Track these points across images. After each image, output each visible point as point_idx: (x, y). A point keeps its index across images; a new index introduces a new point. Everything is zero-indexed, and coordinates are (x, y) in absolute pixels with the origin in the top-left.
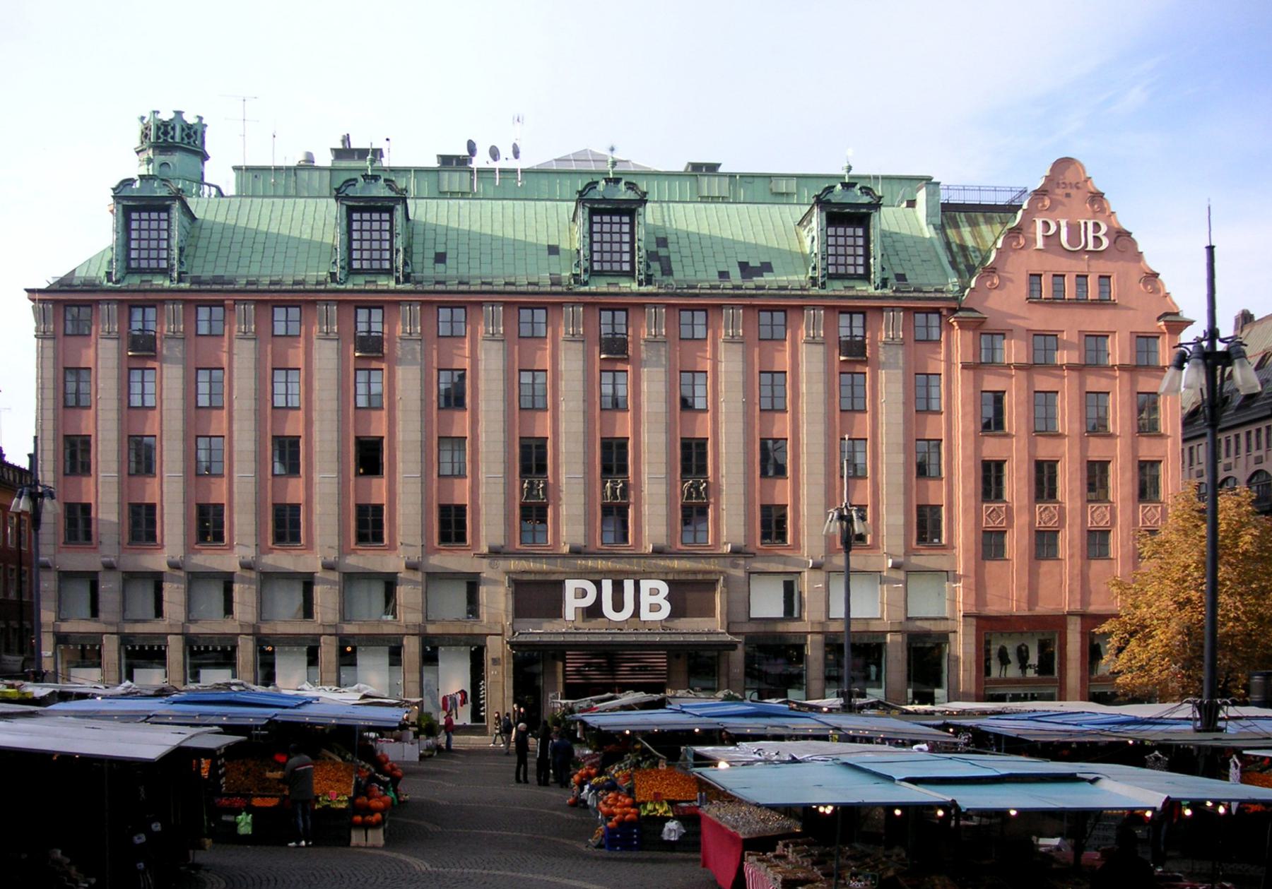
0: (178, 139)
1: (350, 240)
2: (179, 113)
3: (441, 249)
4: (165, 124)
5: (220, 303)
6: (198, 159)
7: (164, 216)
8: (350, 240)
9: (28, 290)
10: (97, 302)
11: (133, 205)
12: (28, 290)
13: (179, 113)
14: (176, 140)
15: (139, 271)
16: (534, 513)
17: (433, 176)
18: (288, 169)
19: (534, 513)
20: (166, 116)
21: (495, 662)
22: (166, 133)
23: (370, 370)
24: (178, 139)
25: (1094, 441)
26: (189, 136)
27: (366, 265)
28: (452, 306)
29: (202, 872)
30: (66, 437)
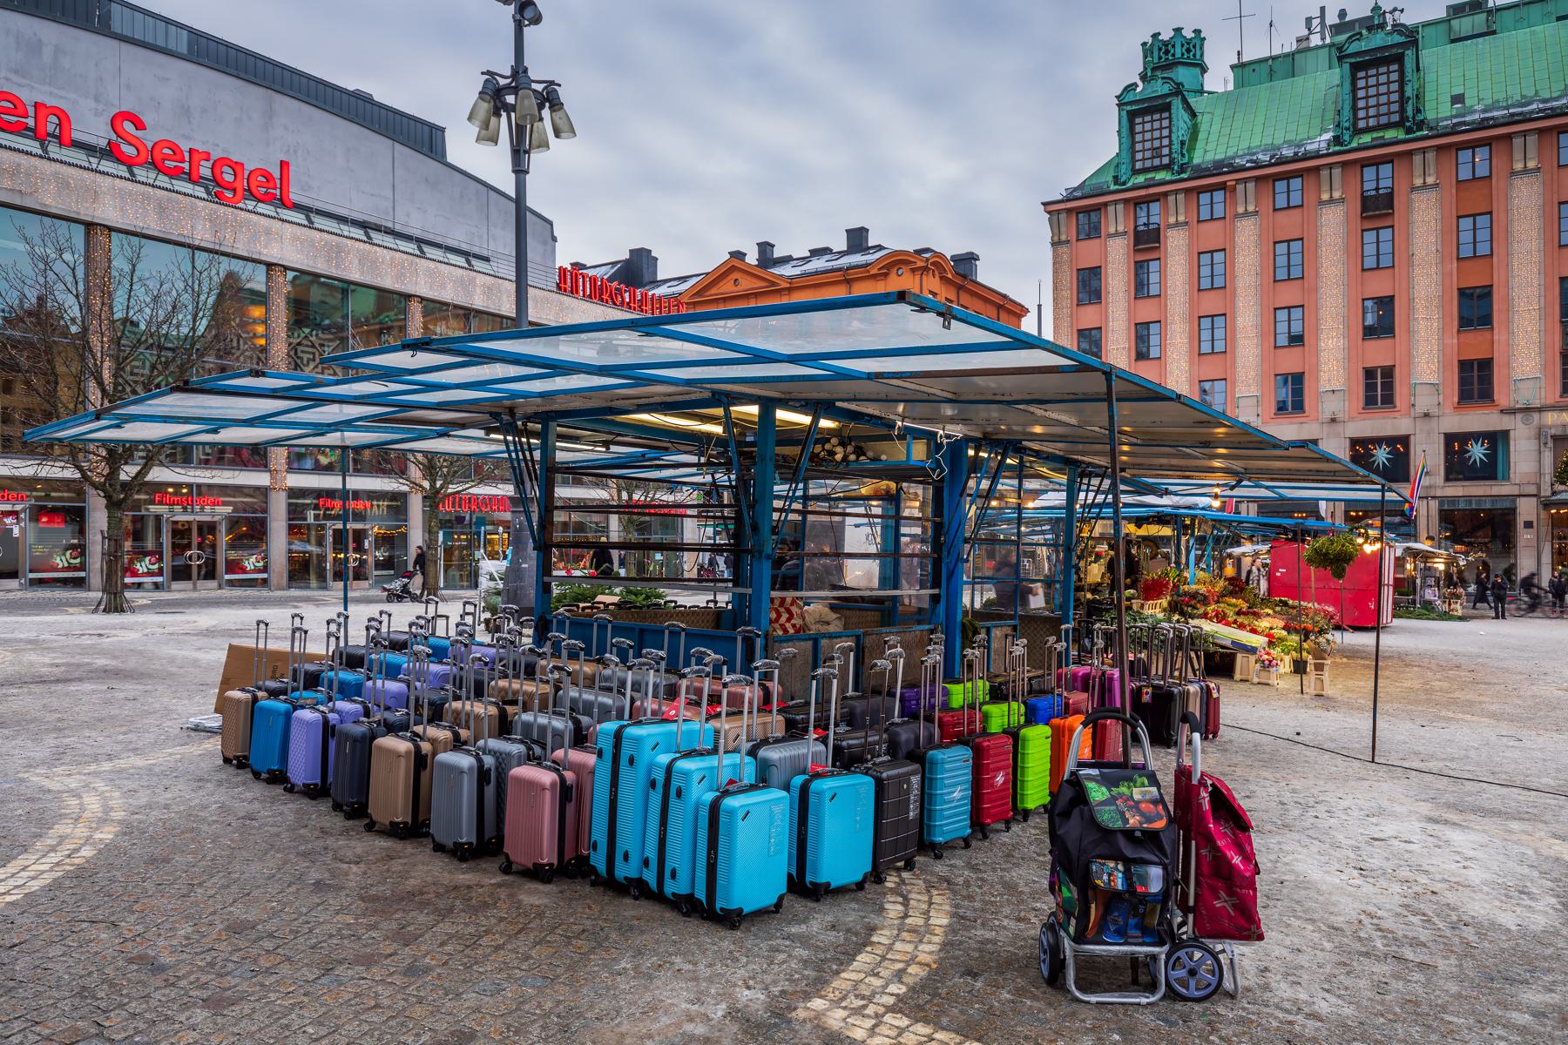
0: (1178, 55)
1: (1355, 99)
2: (1178, 30)
3: (1457, 91)
4: (1166, 44)
5: (1222, 186)
6: (1198, 70)
7: (1166, 115)
8: (1355, 99)
9: (1044, 204)
10: (1106, 204)
11: (1138, 111)
12: (1044, 204)
13: (1178, 30)
14: (1173, 57)
15: (1144, 171)
16: (195, 539)
17: (1443, 27)
18: (1286, 55)
19: (195, 539)
20: (1166, 35)
21: (1528, 525)
22: (1167, 52)
23: (1377, 229)
24: (1178, 55)
25: (1295, 368)
26: (1188, 51)
27: (1372, 122)
28: (1473, 145)
29: (1009, 631)
30: (1080, 331)
